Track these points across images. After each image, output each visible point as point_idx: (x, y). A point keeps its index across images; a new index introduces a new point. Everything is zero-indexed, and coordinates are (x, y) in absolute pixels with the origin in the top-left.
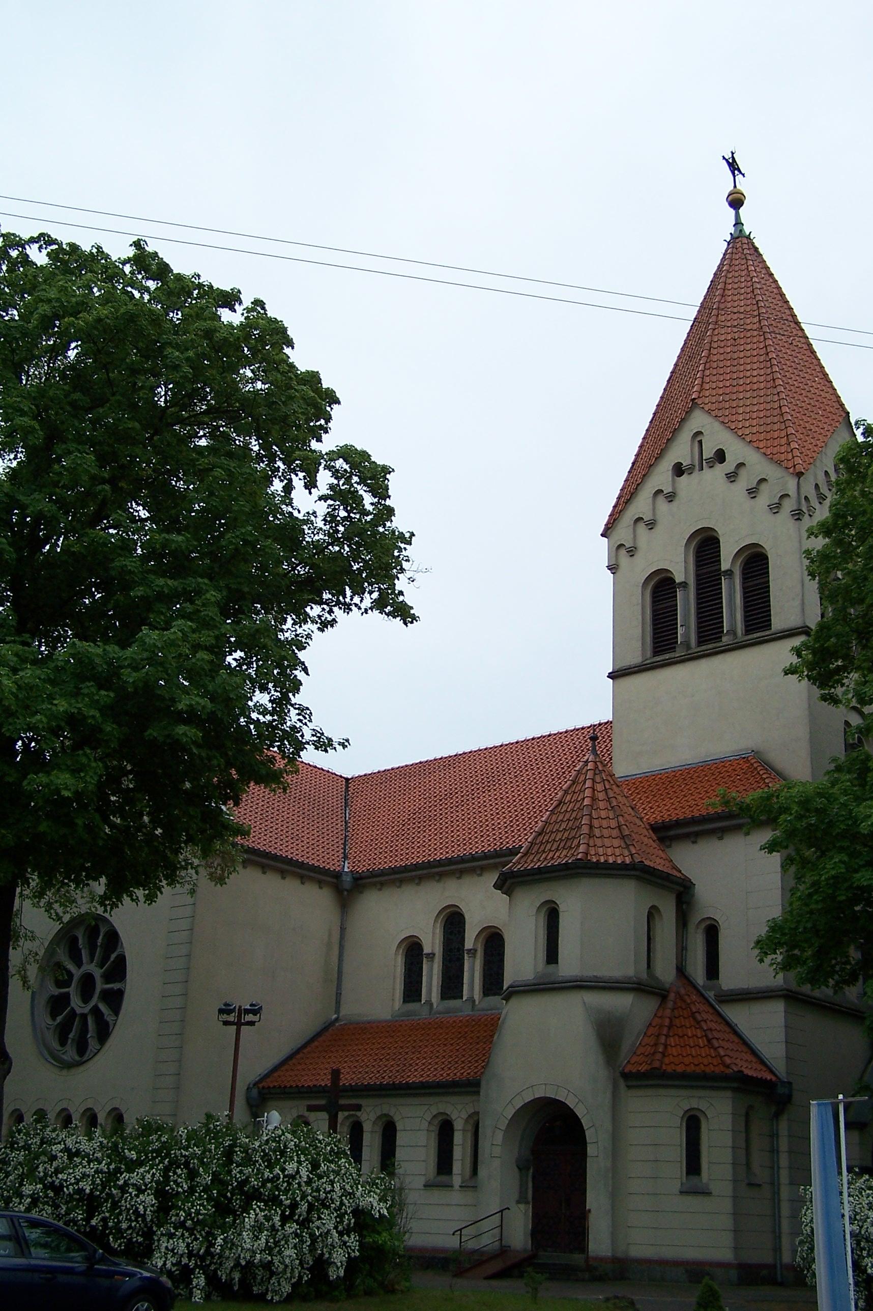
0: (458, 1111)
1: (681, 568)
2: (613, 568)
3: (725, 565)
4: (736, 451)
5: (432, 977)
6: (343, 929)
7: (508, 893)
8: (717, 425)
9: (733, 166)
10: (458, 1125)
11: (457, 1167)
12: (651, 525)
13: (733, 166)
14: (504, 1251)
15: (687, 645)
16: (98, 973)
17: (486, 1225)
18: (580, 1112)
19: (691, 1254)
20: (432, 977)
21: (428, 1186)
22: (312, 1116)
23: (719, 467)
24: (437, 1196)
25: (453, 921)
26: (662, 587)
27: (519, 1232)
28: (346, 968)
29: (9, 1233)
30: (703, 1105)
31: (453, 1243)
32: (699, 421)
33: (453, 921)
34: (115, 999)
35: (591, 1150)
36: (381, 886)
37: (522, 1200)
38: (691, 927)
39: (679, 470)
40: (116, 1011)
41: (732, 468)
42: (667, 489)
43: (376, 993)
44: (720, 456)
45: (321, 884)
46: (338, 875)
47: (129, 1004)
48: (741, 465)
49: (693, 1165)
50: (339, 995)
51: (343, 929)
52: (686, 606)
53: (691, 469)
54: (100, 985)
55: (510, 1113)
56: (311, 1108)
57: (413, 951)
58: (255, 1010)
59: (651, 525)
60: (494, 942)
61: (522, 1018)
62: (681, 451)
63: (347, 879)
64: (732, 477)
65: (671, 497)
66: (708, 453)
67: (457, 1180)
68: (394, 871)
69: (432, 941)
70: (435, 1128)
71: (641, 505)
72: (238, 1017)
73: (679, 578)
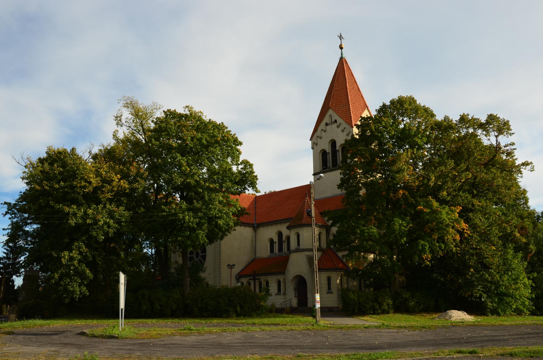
0: (281, 278)
1: (328, 149)
2: (313, 148)
3: (337, 149)
4: (339, 120)
5: (276, 247)
6: (255, 237)
7: (289, 230)
8: (335, 114)
9: (341, 37)
10: (282, 281)
11: (282, 290)
12: (321, 138)
13: (341, 37)
14: (292, 307)
15: (330, 167)
16: (199, 251)
17: (288, 302)
18: (305, 277)
19: (329, 306)
20: (276, 247)
21: (276, 295)
22: (250, 281)
23: (335, 124)
24: (278, 297)
25: (280, 234)
26: (324, 153)
27: (295, 302)
28: (257, 246)
29: (336, 305)
30: (331, 275)
31: (280, 306)
32: (330, 112)
33: (280, 234)
34: (204, 257)
35: (308, 286)
36: (263, 226)
37: (295, 297)
38: (330, 235)
39: (327, 124)
40: (205, 260)
41: (338, 125)
42: (324, 129)
43: (264, 252)
44: (336, 121)
45: (249, 227)
46: (253, 224)
47: (207, 259)
48: (340, 124)
49: (329, 288)
50: (255, 252)
51: (255, 237)
52: (330, 157)
53: (329, 125)
54: (200, 254)
55: (291, 278)
56: (250, 279)
57: (272, 241)
58: (234, 265)
59: (321, 138)
60: (288, 238)
61: (294, 257)
62: (326, 119)
63: (256, 225)
64: (338, 127)
65: (325, 131)
66: (333, 120)
67: (282, 293)
68: (266, 223)
69: (276, 239)
70: (277, 282)
71: (319, 132)
72: (231, 267)
73: (327, 151)
